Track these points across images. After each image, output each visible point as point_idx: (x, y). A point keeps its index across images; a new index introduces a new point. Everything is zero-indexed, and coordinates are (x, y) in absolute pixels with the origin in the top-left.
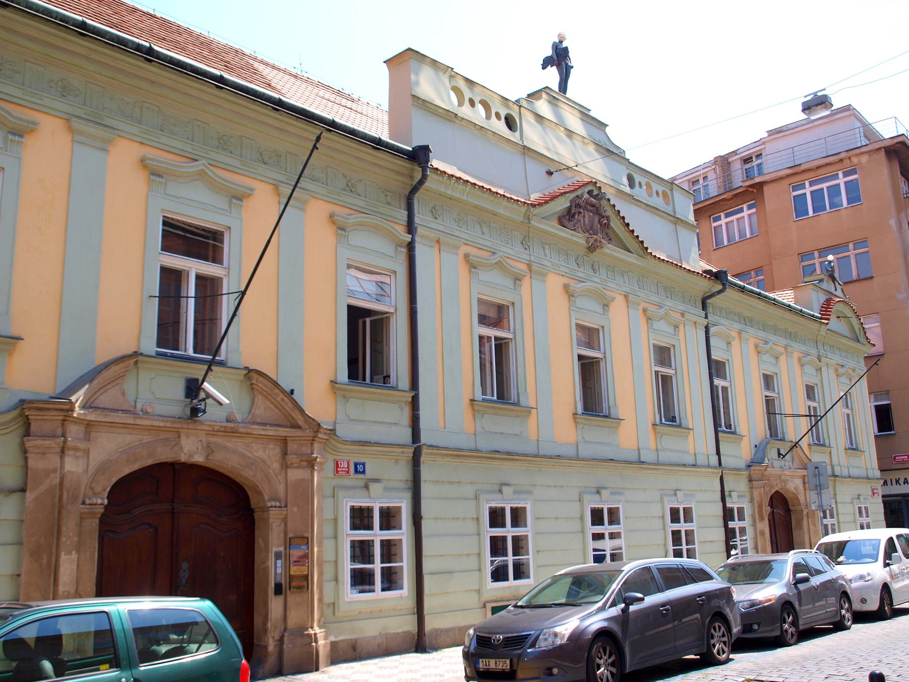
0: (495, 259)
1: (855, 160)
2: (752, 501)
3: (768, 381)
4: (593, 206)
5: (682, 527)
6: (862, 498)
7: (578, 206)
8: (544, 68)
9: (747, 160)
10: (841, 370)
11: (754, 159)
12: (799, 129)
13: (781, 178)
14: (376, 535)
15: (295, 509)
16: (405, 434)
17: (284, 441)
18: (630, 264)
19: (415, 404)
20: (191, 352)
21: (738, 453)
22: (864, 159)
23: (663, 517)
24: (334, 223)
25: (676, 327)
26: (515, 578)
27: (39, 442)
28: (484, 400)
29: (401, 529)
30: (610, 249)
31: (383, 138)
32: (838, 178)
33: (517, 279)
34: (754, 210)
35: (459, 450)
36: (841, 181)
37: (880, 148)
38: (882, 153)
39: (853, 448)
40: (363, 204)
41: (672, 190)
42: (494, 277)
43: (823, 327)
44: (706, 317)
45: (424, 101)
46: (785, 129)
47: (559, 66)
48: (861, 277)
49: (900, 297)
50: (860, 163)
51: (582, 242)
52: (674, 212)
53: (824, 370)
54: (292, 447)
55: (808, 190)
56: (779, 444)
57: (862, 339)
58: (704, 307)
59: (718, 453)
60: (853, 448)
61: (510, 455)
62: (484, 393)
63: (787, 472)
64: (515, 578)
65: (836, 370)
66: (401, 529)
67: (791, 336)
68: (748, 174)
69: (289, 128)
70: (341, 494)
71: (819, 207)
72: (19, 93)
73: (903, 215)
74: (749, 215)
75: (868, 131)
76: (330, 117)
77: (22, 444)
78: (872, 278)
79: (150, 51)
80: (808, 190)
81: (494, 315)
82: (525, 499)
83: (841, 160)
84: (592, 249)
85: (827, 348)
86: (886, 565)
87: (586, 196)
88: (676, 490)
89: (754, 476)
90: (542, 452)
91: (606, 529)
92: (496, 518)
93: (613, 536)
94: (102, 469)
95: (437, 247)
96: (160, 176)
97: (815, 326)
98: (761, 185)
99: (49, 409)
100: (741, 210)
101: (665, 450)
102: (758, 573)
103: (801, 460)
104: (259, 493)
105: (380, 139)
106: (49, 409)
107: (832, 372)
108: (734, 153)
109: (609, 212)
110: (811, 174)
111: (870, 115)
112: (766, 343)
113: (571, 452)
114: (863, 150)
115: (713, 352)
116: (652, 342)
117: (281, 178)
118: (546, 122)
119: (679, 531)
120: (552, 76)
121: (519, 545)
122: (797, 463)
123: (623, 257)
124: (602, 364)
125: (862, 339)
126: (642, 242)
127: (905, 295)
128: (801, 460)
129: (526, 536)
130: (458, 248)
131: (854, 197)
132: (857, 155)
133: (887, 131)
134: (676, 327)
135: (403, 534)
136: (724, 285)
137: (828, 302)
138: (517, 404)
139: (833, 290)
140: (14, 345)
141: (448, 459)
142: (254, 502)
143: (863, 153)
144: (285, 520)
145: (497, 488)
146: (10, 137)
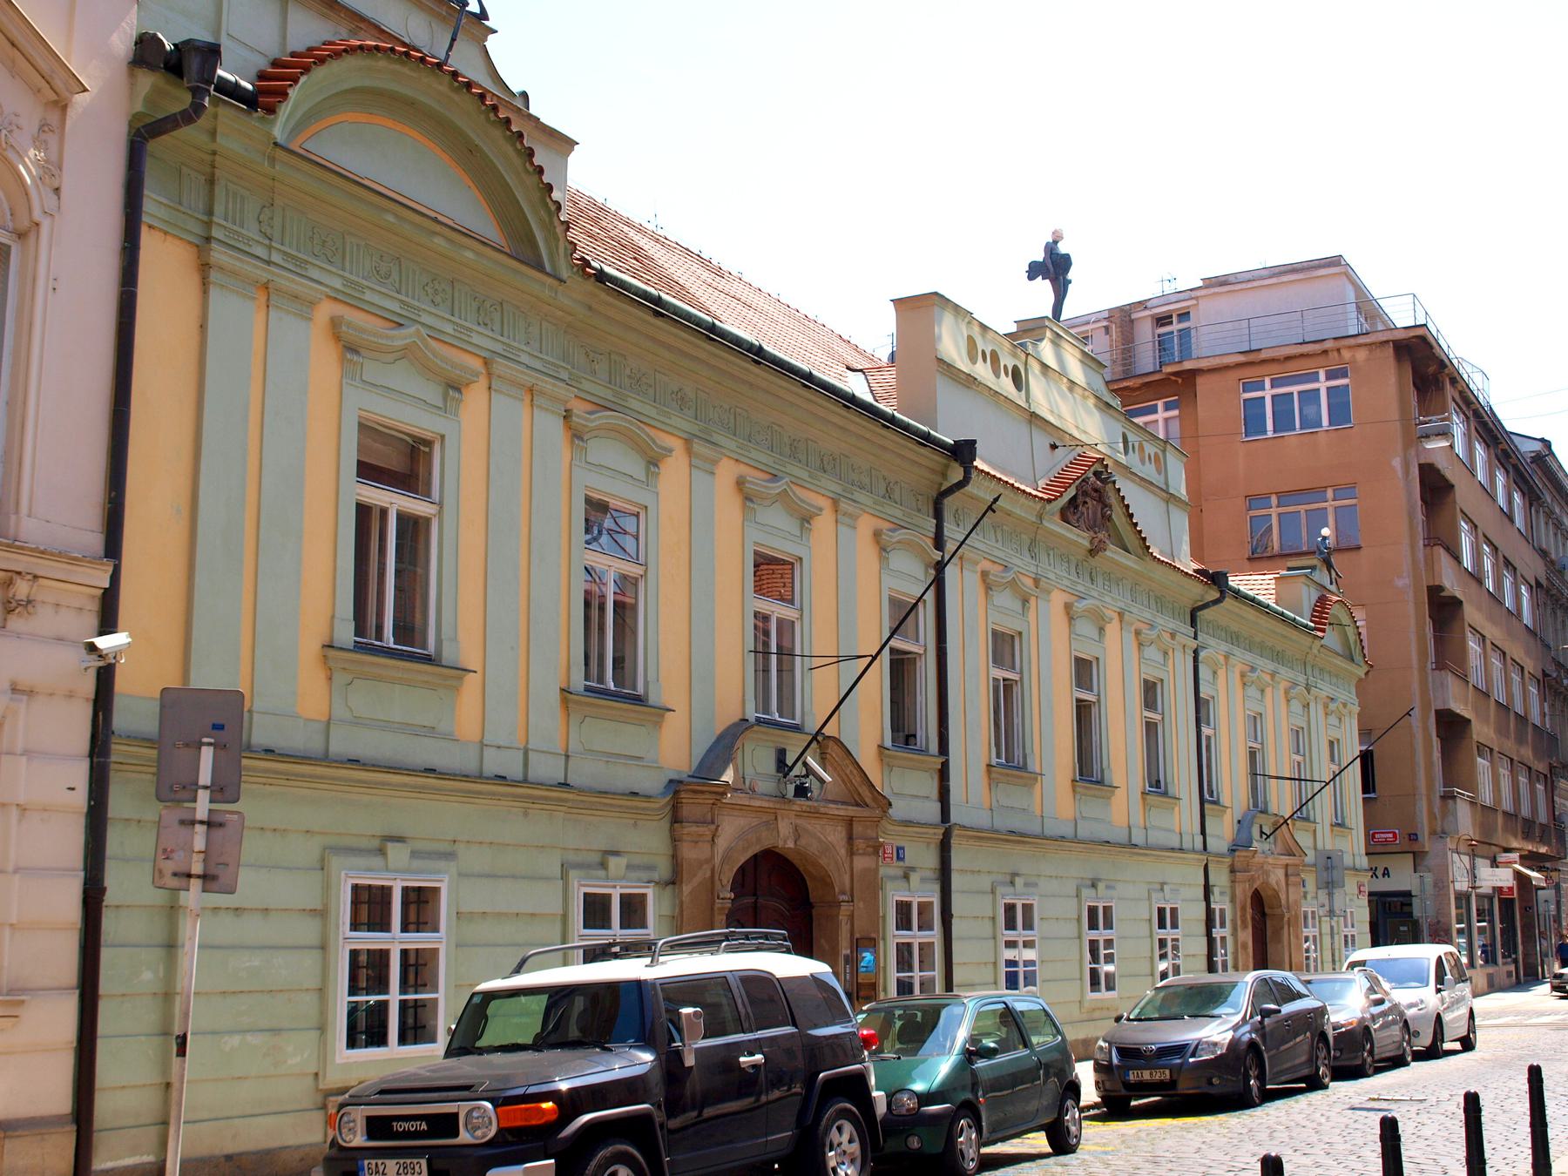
0: (1009, 576)
1: (1346, 354)
2: (1233, 900)
3: (771, 573)
4: (1096, 491)
5: (1101, 935)
6: (1019, 881)
7: (1085, 494)
8: (1031, 277)
9: (1163, 320)
10: (1332, 706)
11: (1175, 319)
12: (1256, 284)
13: (1227, 368)
14: (914, 937)
15: (861, 905)
16: (932, 810)
17: (850, 822)
18: (1128, 568)
19: (944, 774)
20: (389, 639)
21: (1222, 831)
22: (1361, 355)
23: (993, 919)
24: (878, 542)
25: (1166, 653)
26: (403, 1040)
27: (694, 829)
28: (587, 689)
29: (436, 930)
30: (1113, 552)
31: (858, 394)
32: (1317, 380)
33: (454, 387)
34: (1175, 413)
35: (979, 830)
36: (1323, 385)
37: (1387, 342)
38: (1390, 350)
39: (1339, 825)
40: (899, 514)
41: (1164, 451)
42: (402, 378)
43: (1317, 643)
44: (1195, 638)
45: (949, 365)
46: (1232, 279)
47: (1054, 282)
48: (1342, 545)
49: (1400, 583)
50: (1353, 362)
51: (1086, 544)
52: (1167, 484)
53: (1312, 705)
54: (858, 829)
55: (1268, 393)
56: (1261, 819)
57: (1358, 658)
58: (1193, 623)
59: (1203, 832)
60: (1339, 825)
61: (1017, 837)
62: (998, 756)
63: (1270, 860)
64: (403, 1040)
65: (1326, 706)
66: (436, 930)
67: (1278, 656)
68: (1162, 344)
69: (852, 427)
70: (335, 862)
71: (1283, 421)
72: (653, 413)
73: (1412, 452)
74: (1166, 420)
75: (1367, 307)
76: (805, 367)
77: (672, 830)
78: (1359, 548)
79: (658, 301)
80: (1268, 393)
81: (400, 462)
82: (439, 872)
83: (1325, 352)
84: (1093, 552)
85: (1316, 672)
86: (1438, 991)
87: (1093, 479)
88: (1163, 884)
89: (1238, 865)
90: (1048, 832)
91: (1019, 934)
92: (370, 907)
93: (1028, 944)
94: (727, 858)
95: (527, 399)
96: (356, 352)
97: (1307, 640)
98: (1193, 374)
99: (702, 792)
100: (1154, 410)
101: (1154, 827)
102: (1204, 1000)
103: (1285, 842)
104: (826, 882)
105: (760, 348)
106: (702, 792)
107: (1320, 707)
108: (1142, 304)
109: (1113, 500)
110: (1274, 368)
111: (1376, 286)
112: (1253, 669)
113: (315, 745)
114: (1362, 340)
115: (1202, 688)
116: (991, 626)
117: (498, 348)
118: (1051, 373)
119: (909, 945)
120: (1043, 289)
121: (418, 968)
122: (1280, 848)
123: (1123, 560)
124: (1094, 710)
125: (1358, 658)
126: (1144, 539)
127: (1407, 581)
128: (1285, 842)
129: (435, 951)
130: (312, 304)
131: (1340, 411)
132: (1350, 347)
133: (1401, 317)
134: (1025, 601)
135: (935, 936)
136: (1222, 592)
137: (1322, 600)
138: (1100, 782)
139: (1326, 582)
140: (461, 678)
141: (971, 842)
142: (814, 895)
143: (1360, 345)
144: (851, 917)
145: (1008, 878)
146: (349, 356)
